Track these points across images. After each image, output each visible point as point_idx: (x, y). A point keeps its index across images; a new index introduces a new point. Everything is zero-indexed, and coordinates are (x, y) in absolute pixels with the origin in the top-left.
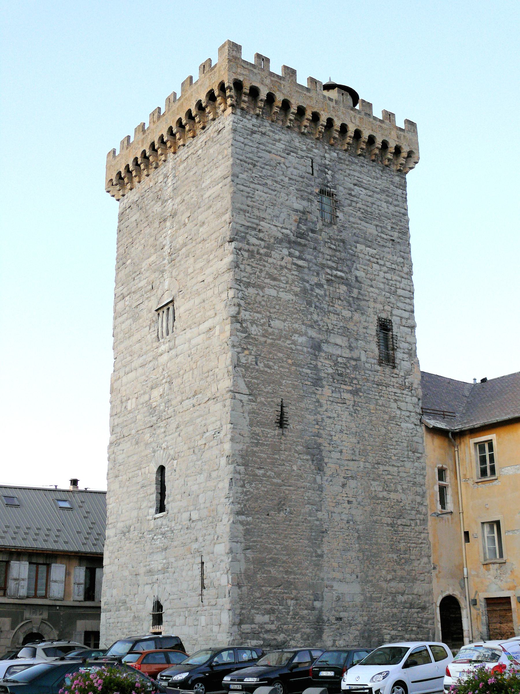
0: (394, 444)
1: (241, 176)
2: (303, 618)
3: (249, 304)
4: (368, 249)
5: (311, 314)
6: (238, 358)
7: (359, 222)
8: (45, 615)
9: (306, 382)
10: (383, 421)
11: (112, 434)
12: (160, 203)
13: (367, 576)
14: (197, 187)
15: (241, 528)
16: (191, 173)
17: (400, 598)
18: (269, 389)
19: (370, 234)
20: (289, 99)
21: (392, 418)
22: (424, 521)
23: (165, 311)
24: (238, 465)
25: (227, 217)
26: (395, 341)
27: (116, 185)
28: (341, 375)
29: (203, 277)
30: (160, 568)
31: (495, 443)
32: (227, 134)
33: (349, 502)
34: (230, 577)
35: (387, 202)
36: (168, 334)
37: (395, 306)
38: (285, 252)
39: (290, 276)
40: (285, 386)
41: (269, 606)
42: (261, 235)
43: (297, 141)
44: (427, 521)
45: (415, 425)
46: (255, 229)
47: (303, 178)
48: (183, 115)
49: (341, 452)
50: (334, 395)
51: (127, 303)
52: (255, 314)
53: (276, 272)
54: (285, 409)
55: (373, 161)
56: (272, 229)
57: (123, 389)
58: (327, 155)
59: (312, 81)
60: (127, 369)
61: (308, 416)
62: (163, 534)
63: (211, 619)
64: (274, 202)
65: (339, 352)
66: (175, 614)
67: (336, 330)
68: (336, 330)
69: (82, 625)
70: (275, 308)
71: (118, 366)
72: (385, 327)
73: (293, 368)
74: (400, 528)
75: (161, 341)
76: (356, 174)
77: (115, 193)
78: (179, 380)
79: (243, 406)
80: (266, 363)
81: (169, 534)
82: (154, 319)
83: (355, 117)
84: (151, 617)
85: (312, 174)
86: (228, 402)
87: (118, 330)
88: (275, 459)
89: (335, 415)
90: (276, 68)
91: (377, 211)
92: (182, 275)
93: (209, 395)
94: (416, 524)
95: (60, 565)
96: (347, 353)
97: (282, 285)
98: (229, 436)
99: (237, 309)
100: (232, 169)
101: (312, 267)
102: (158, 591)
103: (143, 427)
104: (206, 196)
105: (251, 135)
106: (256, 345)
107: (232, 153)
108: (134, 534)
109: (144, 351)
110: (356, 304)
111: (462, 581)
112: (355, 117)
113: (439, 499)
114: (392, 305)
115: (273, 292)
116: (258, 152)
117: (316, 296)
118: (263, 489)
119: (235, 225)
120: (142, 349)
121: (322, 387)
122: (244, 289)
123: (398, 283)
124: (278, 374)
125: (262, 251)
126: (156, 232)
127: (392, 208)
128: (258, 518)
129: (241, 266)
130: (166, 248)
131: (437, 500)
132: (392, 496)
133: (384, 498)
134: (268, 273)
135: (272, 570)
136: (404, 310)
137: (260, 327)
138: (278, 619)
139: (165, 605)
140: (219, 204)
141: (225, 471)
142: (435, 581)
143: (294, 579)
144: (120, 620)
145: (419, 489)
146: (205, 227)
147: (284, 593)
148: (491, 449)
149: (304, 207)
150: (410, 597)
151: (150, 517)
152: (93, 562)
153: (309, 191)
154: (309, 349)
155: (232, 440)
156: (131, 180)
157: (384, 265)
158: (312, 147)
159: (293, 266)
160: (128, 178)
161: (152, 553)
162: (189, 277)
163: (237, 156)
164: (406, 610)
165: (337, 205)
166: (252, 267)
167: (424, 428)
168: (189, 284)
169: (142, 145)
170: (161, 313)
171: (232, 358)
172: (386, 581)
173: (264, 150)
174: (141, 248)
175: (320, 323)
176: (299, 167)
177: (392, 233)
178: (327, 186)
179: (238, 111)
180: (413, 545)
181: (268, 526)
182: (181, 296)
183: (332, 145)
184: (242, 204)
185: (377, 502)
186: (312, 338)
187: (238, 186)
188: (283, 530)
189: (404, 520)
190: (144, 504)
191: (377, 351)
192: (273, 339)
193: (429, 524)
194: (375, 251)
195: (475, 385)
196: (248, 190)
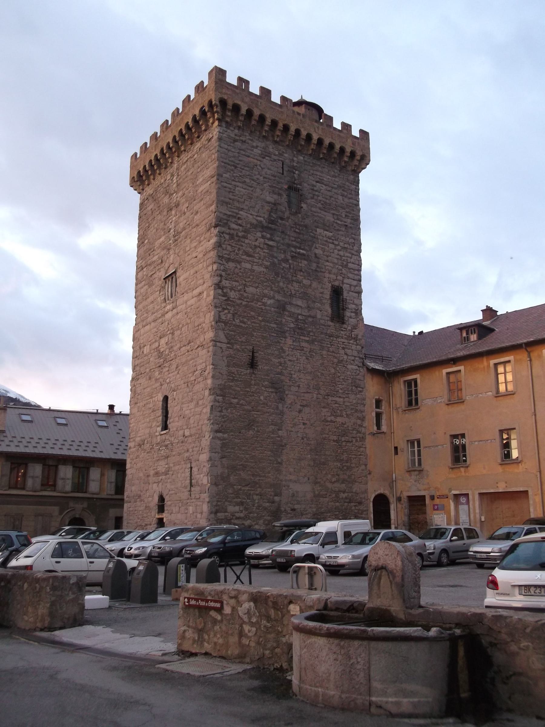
0: (341, 380)
1: (224, 175)
2: (265, 509)
3: (229, 275)
4: (325, 232)
5: (278, 282)
6: (219, 316)
7: (319, 211)
8: (85, 505)
9: (273, 334)
10: (333, 364)
11: (133, 372)
12: (168, 196)
13: (317, 479)
14: (193, 184)
15: (219, 442)
16: (190, 173)
17: (343, 495)
18: (243, 339)
19: (328, 221)
20: (264, 113)
21: (340, 362)
22: (363, 439)
23: (170, 280)
24: (218, 396)
25: (213, 207)
26: (344, 303)
27: (137, 181)
28: (300, 329)
29: (197, 254)
30: (163, 471)
31: (419, 381)
32: (214, 142)
33: (304, 424)
34: (209, 478)
35: (343, 195)
36: (172, 297)
37: (346, 276)
38: (259, 234)
39: (262, 254)
40: (256, 337)
41: (239, 500)
42: (240, 222)
43: (271, 148)
44: (365, 439)
45: (359, 367)
46: (235, 217)
47: (275, 177)
48: (183, 127)
49: (299, 386)
50: (294, 344)
51: (144, 273)
52: (234, 283)
53: (251, 250)
54: (255, 354)
55: (333, 163)
56: (248, 217)
57: (141, 338)
58: (295, 159)
59: (283, 98)
60: (144, 323)
61: (273, 360)
62: (166, 446)
63: (196, 509)
64: (251, 196)
65: (299, 311)
66: (173, 505)
67: (298, 294)
68: (298, 294)
69: (113, 513)
70: (249, 277)
71: (138, 322)
72: (337, 292)
73: (263, 323)
74: (344, 444)
75: (167, 302)
76: (318, 173)
77: (137, 187)
78: (179, 332)
79: (222, 351)
80: (241, 319)
81: (170, 446)
82: (163, 285)
83: (318, 128)
84: (157, 507)
85: (283, 174)
86: (211, 349)
87: (138, 293)
88: (246, 391)
89: (295, 359)
90: (254, 89)
91: (334, 203)
92: (182, 252)
93: (198, 343)
94: (357, 441)
95: (97, 469)
96: (306, 312)
97: (256, 260)
98: (211, 374)
99: (219, 278)
100: (218, 170)
101: (280, 246)
102: (162, 488)
103: (154, 367)
104: (199, 191)
105: (234, 143)
106: (234, 306)
107: (218, 157)
108: (147, 446)
109: (155, 309)
110: (316, 274)
111: (392, 484)
112: (318, 128)
113: (375, 422)
114: (343, 276)
115: (248, 266)
116: (239, 156)
117: (283, 269)
118: (236, 413)
119: (219, 214)
120: (154, 308)
121: (285, 338)
122: (225, 263)
123: (349, 259)
124: (250, 328)
125: (240, 234)
126: (165, 219)
127: (346, 200)
128: (232, 435)
129: (223, 246)
130: (172, 231)
131: (373, 423)
132: (339, 419)
133: (331, 421)
134: (244, 251)
135: (241, 472)
136: (354, 280)
137: (237, 292)
138: (246, 509)
139: (167, 498)
140: (208, 199)
141: (208, 399)
142: (370, 483)
143: (259, 480)
144: (136, 508)
145: (359, 415)
146: (198, 215)
147: (251, 490)
148: (416, 385)
149: (275, 200)
150: (350, 495)
151: (157, 434)
152: (120, 466)
153: (280, 187)
154: (276, 309)
155: (213, 377)
156: (148, 177)
157: (338, 245)
158: (283, 152)
159: (265, 246)
160: (146, 177)
161: (159, 460)
162: (187, 254)
163: (221, 159)
164: (346, 504)
165: (301, 198)
166: (232, 246)
167: (365, 369)
168: (187, 259)
169: (155, 150)
170: (167, 281)
171: (214, 316)
172: (331, 482)
173: (244, 155)
174: (155, 230)
175: (285, 289)
176: (272, 168)
177: (346, 220)
178: (294, 183)
179: (224, 124)
180: (353, 456)
181: (239, 441)
182: (181, 268)
183: (299, 151)
184: (225, 197)
185: (326, 424)
186: (278, 301)
187: (222, 184)
188: (252, 444)
189: (347, 438)
190: (154, 424)
191: (330, 310)
192: (247, 301)
193: (367, 440)
194: (331, 234)
195: (414, 336)
196: (230, 186)
